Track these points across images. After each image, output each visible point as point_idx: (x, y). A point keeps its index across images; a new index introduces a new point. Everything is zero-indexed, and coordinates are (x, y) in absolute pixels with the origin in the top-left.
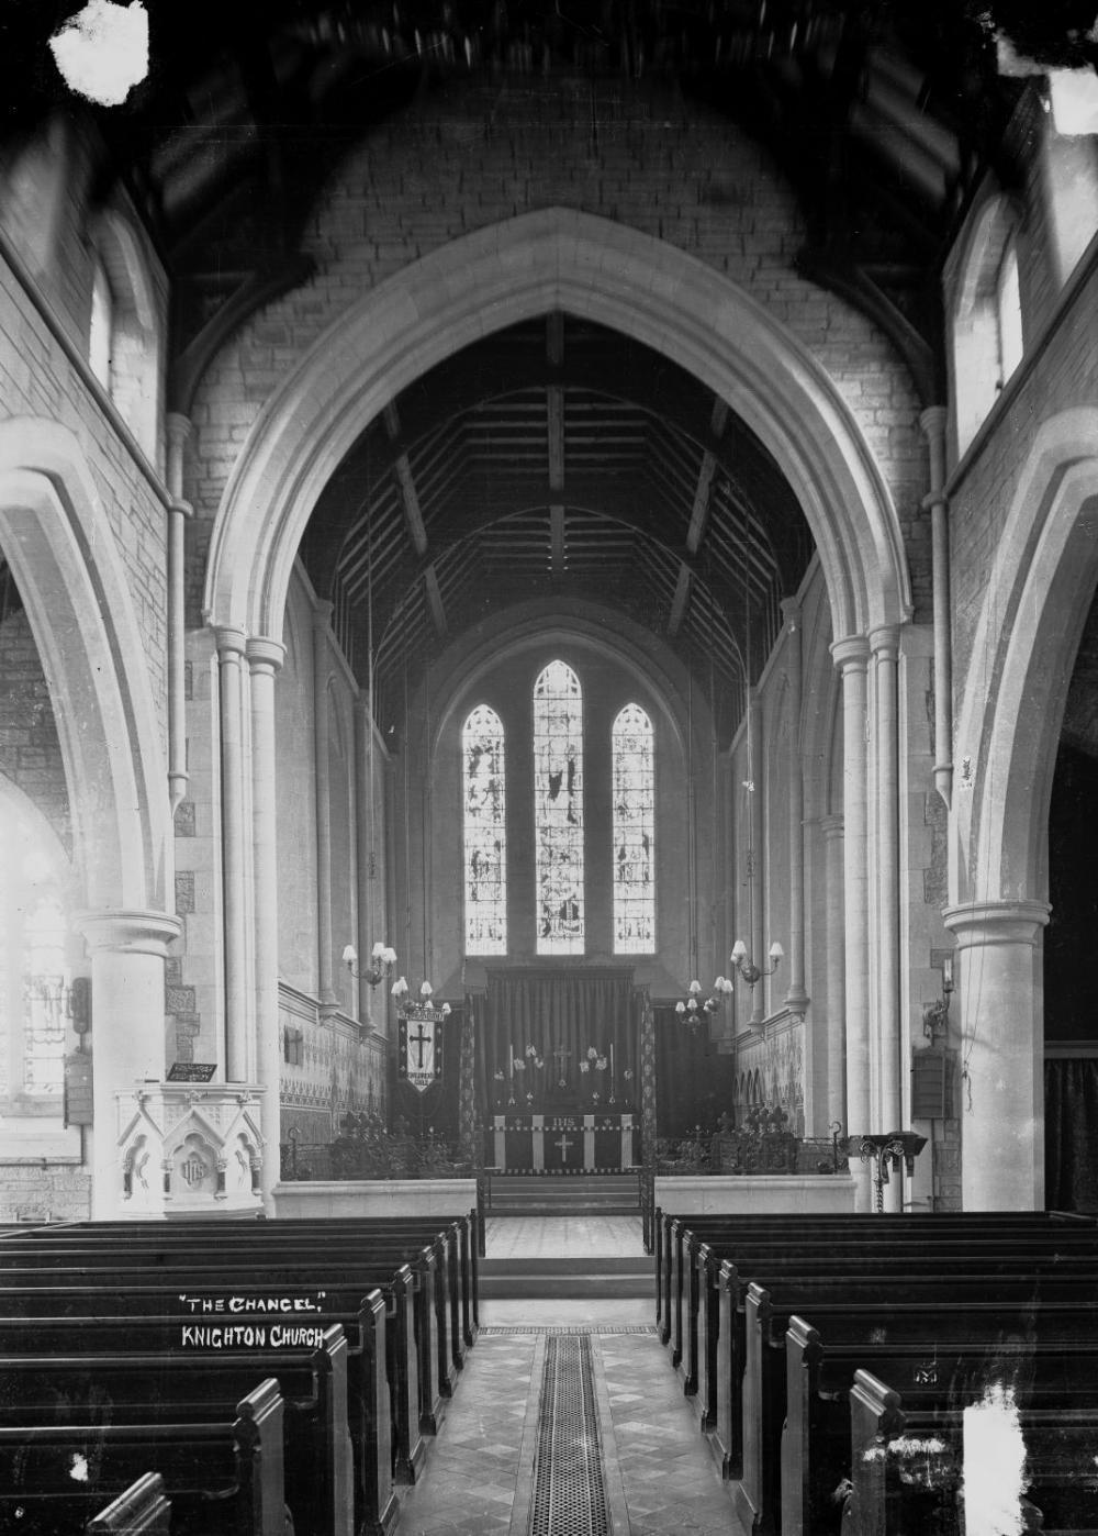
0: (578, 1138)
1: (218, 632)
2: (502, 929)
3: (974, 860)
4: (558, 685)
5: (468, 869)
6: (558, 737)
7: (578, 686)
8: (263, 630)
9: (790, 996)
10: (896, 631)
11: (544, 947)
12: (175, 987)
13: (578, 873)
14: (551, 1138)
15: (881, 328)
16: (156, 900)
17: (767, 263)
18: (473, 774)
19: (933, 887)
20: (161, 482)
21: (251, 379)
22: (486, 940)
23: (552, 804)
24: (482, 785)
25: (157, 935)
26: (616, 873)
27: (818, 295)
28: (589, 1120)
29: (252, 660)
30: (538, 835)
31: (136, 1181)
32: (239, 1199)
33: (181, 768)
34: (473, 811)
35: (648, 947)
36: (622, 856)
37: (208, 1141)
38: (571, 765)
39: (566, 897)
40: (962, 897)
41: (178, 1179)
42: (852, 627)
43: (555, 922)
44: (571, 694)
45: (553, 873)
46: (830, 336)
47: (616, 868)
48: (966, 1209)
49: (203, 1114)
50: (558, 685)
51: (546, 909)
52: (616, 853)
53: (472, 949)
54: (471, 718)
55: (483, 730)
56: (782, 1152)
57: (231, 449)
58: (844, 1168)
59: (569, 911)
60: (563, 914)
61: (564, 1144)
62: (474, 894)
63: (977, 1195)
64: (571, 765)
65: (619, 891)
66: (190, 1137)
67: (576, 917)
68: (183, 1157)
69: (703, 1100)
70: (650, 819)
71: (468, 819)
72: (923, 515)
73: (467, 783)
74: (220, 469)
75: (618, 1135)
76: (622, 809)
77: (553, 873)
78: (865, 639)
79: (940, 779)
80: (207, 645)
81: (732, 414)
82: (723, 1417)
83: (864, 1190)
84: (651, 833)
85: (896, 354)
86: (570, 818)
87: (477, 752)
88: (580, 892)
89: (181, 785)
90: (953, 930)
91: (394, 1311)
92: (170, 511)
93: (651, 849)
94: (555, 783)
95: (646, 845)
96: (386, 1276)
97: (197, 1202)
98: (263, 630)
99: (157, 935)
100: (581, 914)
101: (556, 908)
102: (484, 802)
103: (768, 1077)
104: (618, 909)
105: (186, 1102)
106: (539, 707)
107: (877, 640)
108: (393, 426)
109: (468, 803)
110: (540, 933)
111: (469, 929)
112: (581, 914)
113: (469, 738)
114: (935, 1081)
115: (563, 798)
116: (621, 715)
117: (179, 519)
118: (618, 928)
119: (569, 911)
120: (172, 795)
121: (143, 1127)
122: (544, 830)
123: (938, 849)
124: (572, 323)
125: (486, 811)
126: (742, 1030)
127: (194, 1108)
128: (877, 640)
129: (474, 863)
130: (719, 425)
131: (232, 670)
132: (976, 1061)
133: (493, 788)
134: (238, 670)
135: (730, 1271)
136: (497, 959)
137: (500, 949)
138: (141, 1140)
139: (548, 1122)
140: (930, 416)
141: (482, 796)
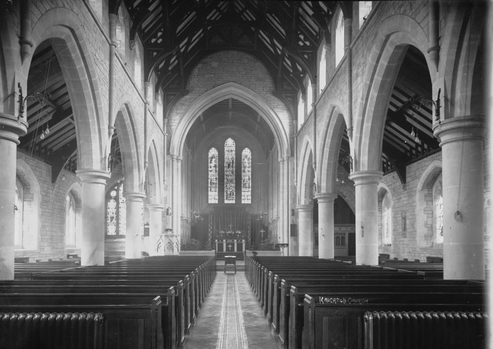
0: (233, 245)
2: (217, 197)
3: (300, 197)
4: (230, 143)
5: (209, 184)
7: (234, 144)
8: (179, 155)
10: (288, 158)
11: (226, 202)
13: (234, 185)
14: (227, 244)
16: (161, 203)
17: (267, 93)
18: (211, 163)
20: (163, 130)
22: (213, 200)
23: (228, 170)
24: (213, 164)
25: (161, 208)
26: (242, 185)
27: (276, 99)
28: (235, 241)
29: (177, 160)
31: (159, 250)
32: (176, 252)
33: (165, 179)
34: (211, 171)
35: (250, 202)
38: (233, 161)
39: (231, 190)
40: (299, 204)
41: (166, 250)
42: (281, 157)
44: (233, 146)
45: (228, 185)
46: (278, 106)
49: (171, 239)
50: (230, 143)
51: (227, 193)
52: (242, 181)
53: (210, 202)
54: (211, 150)
55: (213, 153)
57: (175, 124)
58: (280, 250)
60: (230, 194)
61: (230, 246)
62: (211, 190)
63: (301, 254)
64: (233, 161)
66: (169, 243)
67: (233, 195)
68: (167, 246)
69: (258, 233)
70: (250, 173)
71: (210, 173)
72: (293, 138)
73: (209, 165)
74: (173, 127)
75: (223, 244)
76: (244, 171)
77: (228, 185)
78: (283, 158)
79: (295, 183)
80: (170, 158)
81: (261, 116)
82: (275, 320)
85: (289, 110)
86: (232, 173)
87: (212, 158)
89: (165, 182)
90: (298, 209)
91: (177, 295)
92: (164, 135)
93: (250, 180)
96: (175, 283)
97: (170, 253)
98: (179, 155)
99: (161, 208)
100: (235, 194)
101: (229, 193)
103: (273, 232)
104: (243, 193)
105: (168, 237)
106: (226, 149)
107: (285, 159)
108: (202, 119)
109: (210, 169)
111: (209, 197)
112: (235, 194)
113: (210, 155)
115: (231, 169)
116: (244, 150)
118: (243, 198)
120: (164, 184)
121: (161, 241)
122: (226, 175)
123: (295, 195)
124: (233, 100)
127: (170, 238)
128: (285, 159)
129: (211, 183)
130: (259, 120)
131: (174, 162)
133: (215, 166)
134: (175, 162)
135: (284, 283)
137: (217, 202)
138: (160, 243)
139: (226, 241)
141: (213, 168)
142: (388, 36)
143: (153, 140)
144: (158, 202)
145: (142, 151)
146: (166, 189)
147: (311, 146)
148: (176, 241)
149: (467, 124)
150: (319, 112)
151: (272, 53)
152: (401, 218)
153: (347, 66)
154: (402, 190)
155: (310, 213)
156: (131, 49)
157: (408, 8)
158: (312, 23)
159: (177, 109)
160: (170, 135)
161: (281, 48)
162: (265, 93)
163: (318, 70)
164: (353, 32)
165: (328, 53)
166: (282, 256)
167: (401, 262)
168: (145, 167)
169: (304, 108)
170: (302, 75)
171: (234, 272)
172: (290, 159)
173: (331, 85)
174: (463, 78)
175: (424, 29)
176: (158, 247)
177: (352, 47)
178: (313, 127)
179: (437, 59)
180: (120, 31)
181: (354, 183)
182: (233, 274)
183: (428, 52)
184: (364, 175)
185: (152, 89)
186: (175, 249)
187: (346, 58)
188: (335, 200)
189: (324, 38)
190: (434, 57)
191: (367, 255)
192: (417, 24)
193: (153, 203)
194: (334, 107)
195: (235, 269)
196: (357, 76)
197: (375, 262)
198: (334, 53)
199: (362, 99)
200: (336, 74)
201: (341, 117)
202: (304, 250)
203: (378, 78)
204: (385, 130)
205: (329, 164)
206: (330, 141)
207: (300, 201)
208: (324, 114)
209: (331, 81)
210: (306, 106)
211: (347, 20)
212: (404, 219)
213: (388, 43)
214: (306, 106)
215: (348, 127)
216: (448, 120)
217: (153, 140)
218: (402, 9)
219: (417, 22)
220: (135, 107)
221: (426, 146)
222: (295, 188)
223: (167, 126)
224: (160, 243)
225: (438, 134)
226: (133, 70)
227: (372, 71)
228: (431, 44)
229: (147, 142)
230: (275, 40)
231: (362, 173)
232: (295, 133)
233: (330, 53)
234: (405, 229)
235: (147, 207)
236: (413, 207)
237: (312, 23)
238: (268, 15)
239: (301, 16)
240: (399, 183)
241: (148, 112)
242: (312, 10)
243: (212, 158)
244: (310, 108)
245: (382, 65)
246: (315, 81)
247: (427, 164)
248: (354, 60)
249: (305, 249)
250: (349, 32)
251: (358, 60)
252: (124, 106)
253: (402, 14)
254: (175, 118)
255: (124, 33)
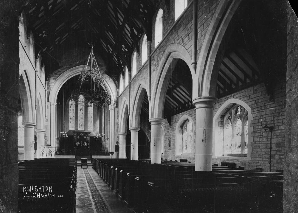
1: (50, 102)
2: (74, 127)
5: (70, 119)
6: (81, 106)
8: (55, 102)
9: (107, 138)
12: (45, 136)
15: (114, 81)
17: (104, 73)
19: (117, 131)
20: (45, 87)
21: (54, 78)
25: (44, 131)
29: (53, 105)
30: (79, 115)
31: (43, 155)
32: (53, 157)
33: (46, 115)
34: (71, 112)
36: (89, 119)
37: (50, 151)
38: (83, 108)
43: (81, 126)
45: (80, 120)
47: (88, 120)
48: (120, 158)
49: (50, 149)
51: (80, 125)
52: (88, 118)
56: (108, 154)
58: (109, 155)
59: (82, 125)
62: (71, 122)
64: (83, 108)
65: (88, 123)
73: (70, 109)
79: (118, 121)
83: (114, 157)
84: (92, 116)
87: (71, 105)
88: (84, 123)
89: (46, 117)
94: (81, 110)
95: (92, 118)
97: (50, 157)
98: (55, 102)
100: (84, 125)
102: (72, 111)
108: (80, 83)
109: (70, 111)
110: (79, 127)
112: (84, 125)
114: (117, 148)
117: (47, 91)
119: (82, 125)
125: (72, 112)
126: (102, 140)
128: (113, 109)
132: (120, 146)
133: (73, 110)
136: (73, 130)
137: (74, 129)
138: (44, 151)
140: (118, 89)
142: (170, 53)
143: (40, 93)
144: (42, 128)
145: (34, 99)
146: (47, 121)
147: (127, 102)
148: (53, 150)
149: (207, 100)
150: (132, 86)
151: (107, 52)
152: (168, 141)
153: (149, 64)
154: (169, 127)
155: (125, 137)
156: (28, 38)
157: (182, 41)
158: (130, 41)
159: (53, 76)
160: (49, 91)
161: (112, 50)
162: (103, 73)
163: (132, 65)
164: (152, 48)
165: (138, 56)
166: (111, 158)
167: (169, 162)
168: (36, 108)
169: (124, 82)
170: (122, 66)
171: (86, 167)
172: (115, 109)
173: (139, 73)
174: (207, 78)
175: (189, 53)
176: (42, 153)
177: (151, 56)
178: (129, 93)
179: (195, 68)
180: (21, 26)
181: (151, 124)
182: (86, 168)
183: (192, 64)
184: (156, 120)
185: (39, 63)
186: (53, 155)
187: (148, 60)
188: (139, 131)
189: (136, 48)
190: (194, 67)
191: (156, 157)
192: (186, 50)
193: (39, 129)
194: (140, 85)
195: (87, 165)
196: (154, 70)
197: (159, 162)
198: (141, 57)
199: (156, 82)
200: (142, 68)
201: (144, 91)
202: (123, 155)
203: (164, 73)
204: (144, 98)
205: (136, 113)
206: (137, 101)
207: (120, 131)
208: (135, 88)
209: (140, 71)
210: (124, 82)
211: (149, 41)
212: (170, 141)
213: (170, 57)
214: (124, 82)
215: (148, 95)
216: (199, 97)
217: (40, 93)
218: (178, 41)
219: (186, 49)
220: (30, 73)
221: (180, 108)
222: (118, 124)
223: (47, 85)
224: (44, 151)
225: (195, 103)
226: (29, 51)
227: (161, 69)
228: (193, 61)
229: (37, 94)
230: (108, 46)
231: (155, 119)
232: (118, 95)
233: (139, 57)
234: (170, 146)
235: (36, 131)
236: (174, 135)
237: (130, 41)
238: (106, 32)
239: (124, 36)
240: (168, 124)
241: (37, 76)
242: (130, 34)
243: (71, 105)
244: (127, 83)
245: (167, 67)
246: (130, 70)
247: (181, 116)
248: (152, 63)
249: (122, 155)
250: (150, 48)
251: (154, 63)
252: (24, 72)
253: (178, 44)
254: (52, 81)
255: (24, 28)
